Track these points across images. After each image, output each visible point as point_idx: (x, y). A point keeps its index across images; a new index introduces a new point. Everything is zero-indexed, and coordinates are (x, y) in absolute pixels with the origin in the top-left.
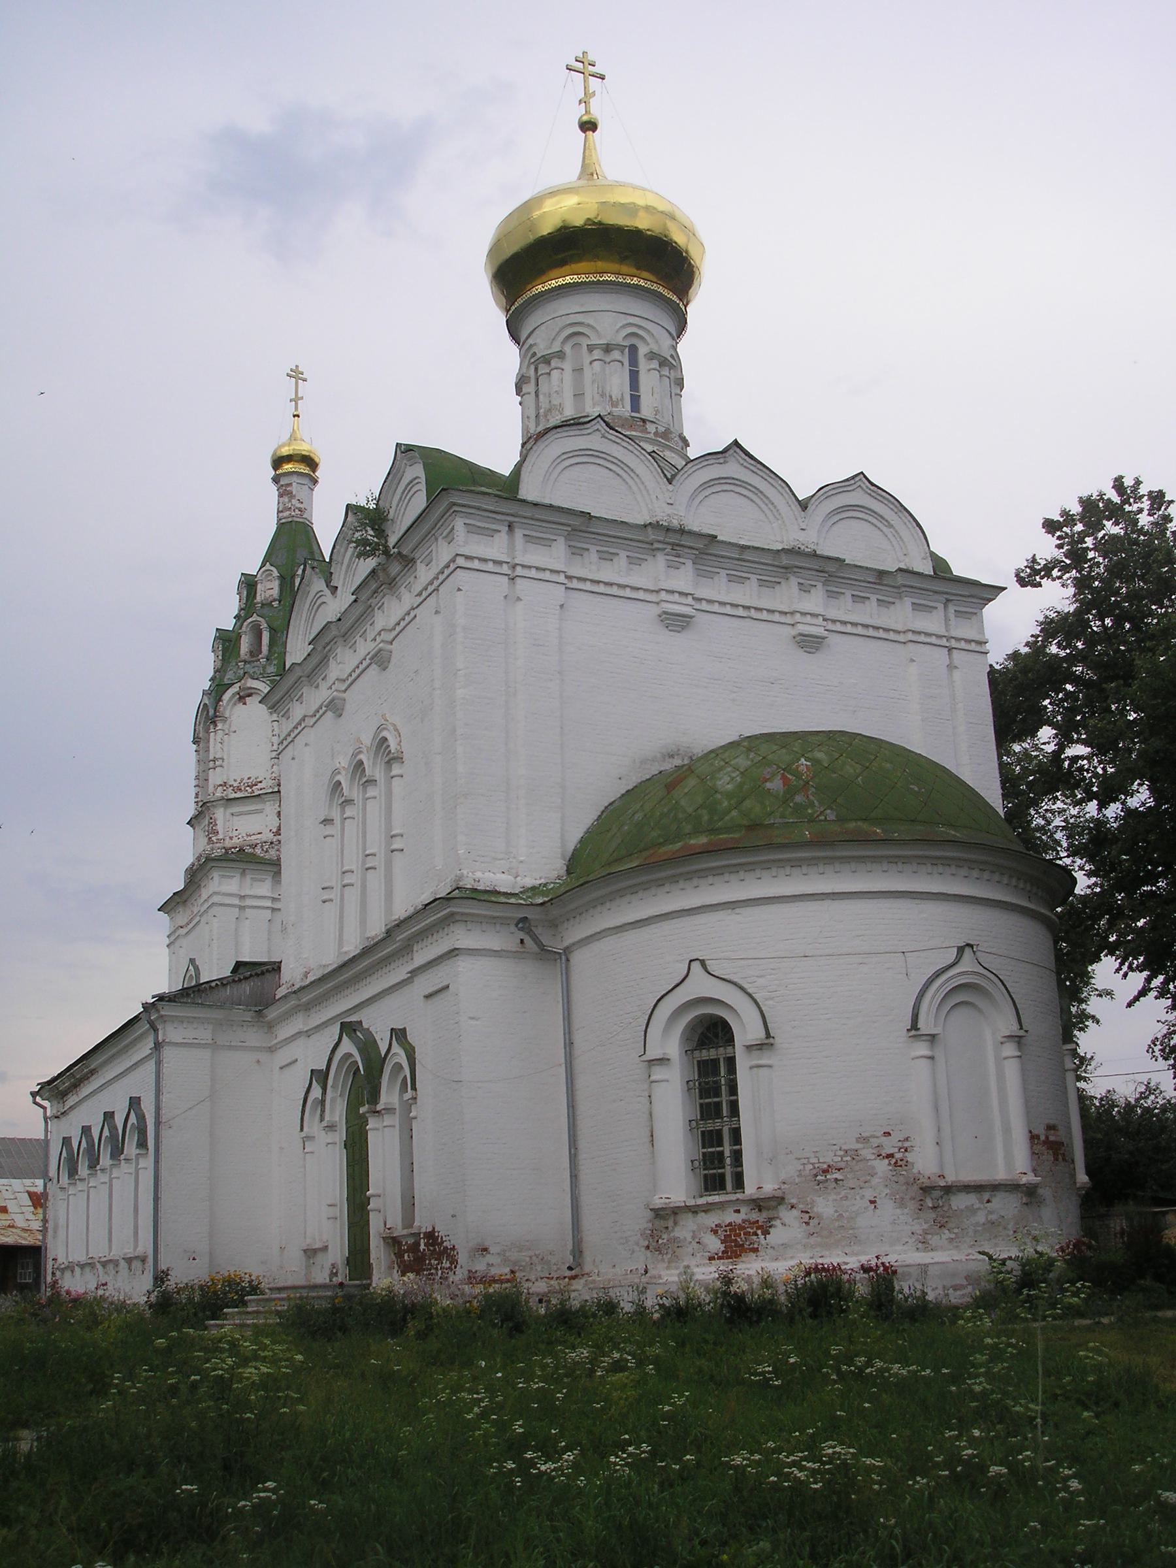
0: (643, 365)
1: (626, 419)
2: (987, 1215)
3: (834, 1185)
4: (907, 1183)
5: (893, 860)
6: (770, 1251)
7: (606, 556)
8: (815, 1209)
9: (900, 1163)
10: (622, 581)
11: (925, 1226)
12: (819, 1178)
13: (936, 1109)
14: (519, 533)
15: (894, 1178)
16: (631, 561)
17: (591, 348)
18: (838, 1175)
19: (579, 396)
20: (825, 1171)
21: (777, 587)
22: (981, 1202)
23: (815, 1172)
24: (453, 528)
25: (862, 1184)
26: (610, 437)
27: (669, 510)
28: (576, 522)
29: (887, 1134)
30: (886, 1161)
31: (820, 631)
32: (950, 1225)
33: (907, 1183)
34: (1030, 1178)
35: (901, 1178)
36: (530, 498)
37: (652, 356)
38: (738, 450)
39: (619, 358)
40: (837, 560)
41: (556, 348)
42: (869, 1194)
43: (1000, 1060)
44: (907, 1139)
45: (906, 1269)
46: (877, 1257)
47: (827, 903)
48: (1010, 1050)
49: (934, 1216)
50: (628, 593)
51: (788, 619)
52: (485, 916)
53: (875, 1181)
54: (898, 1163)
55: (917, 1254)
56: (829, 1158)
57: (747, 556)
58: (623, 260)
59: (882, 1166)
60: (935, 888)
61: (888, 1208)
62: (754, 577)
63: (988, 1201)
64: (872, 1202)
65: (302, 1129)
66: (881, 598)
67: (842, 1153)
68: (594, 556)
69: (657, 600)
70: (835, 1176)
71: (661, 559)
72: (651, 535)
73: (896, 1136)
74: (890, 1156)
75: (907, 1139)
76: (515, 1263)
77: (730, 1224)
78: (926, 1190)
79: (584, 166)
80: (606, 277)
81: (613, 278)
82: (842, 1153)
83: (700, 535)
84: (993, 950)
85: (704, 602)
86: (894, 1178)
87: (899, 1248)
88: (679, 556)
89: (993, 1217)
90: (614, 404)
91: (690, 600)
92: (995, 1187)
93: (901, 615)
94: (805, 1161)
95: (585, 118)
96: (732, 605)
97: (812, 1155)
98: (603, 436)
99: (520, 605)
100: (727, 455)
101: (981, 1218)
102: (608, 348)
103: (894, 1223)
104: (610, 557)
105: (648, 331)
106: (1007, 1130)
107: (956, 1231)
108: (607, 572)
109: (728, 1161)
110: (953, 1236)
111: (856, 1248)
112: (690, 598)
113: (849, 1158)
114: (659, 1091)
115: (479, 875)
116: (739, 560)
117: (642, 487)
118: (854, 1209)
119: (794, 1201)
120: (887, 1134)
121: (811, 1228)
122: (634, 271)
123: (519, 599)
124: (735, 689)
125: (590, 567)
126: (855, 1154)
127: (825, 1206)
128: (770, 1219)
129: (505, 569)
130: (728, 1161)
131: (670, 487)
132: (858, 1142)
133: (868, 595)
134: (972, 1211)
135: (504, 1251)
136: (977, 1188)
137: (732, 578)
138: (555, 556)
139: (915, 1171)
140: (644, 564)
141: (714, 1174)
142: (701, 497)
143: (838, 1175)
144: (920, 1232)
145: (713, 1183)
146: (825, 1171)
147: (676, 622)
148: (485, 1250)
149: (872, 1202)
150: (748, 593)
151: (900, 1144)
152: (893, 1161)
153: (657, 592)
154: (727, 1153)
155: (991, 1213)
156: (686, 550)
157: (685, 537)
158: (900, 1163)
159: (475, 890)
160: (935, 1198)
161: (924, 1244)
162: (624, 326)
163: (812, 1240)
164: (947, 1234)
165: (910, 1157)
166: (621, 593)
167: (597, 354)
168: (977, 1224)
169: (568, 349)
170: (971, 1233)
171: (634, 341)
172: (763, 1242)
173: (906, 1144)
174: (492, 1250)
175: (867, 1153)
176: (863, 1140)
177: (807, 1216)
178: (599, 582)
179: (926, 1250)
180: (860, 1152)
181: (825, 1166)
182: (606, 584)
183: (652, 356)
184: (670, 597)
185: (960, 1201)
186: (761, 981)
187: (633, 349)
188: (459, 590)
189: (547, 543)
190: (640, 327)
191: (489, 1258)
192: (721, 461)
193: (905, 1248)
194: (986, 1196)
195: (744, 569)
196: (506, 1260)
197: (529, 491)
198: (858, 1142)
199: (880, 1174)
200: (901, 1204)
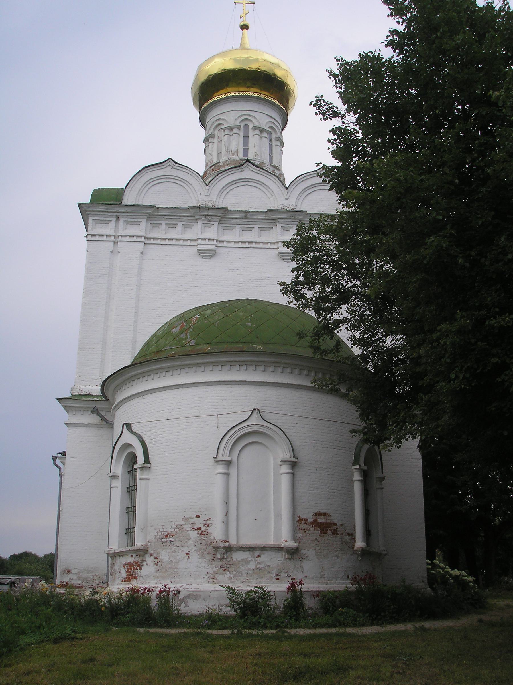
0: (251, 133)
1: (237, 160)
2: (256, 565)
3: (169, 544)
4: (207, 545)
5: (215, 364)
6: (141, 578)
7: (188, 227)
8: (160, 557)
9: (203, 533)
11: (215, 569)
12: (163, 540)
13: (227, 503)
14: (121, 220)
15: (199, 542)
17: (224, 129)
18: (172, 539)
19: (219, 154)
20: (166, 536)
21: (271, 230)
22: (253, 556)
23: (161, 537)
25: (183, 544)
26: (176, 167)
27: (207, 199)
28: (150, 211)
29: (198, 516)
30: (196, 532)
31: (214, 248)
32: (230, 569)
33: (207, 545)
34: (291, 544)
35: (204, 542)
36: (129, 203)
37: (255, 128)
38: (249, 164)
39: (266, 136)
40: (302, 212)
41: (237, 123)
42: (186, 550)
43: (277, 475)
44: (208, 520)
45: (198, 593)
46: (165, 586)
47: (181, 391)
48: (285, 469)
49: (221, 563)
50: (181, 242)
51: (275, 246)
52: (82, 407)
53: (190, 542)
54: (202, 532)
55: (207, 585)
56: (169, 529)
57: (249, 216)
58: (238, 85)
59: (194, 534)
60: (284, 381)
61: (195, 557)
62: (256, 227)
63: (258, 556)
64: (187, 554)
66: (126, 219)
67: (174, 526)
68: (163, 227)
69: (196, 244)
70: (171, 539)
71: (200, 224)
72: (197, 212)
73: (203, 518)
74: (199, 529)
75: (208, 520)
76: (85, 579)
77: (129, 563)
78: (216, 548)
79: (241, 45)
80: (230, 94)
81: (233, 94)
82: (174, 526)
83: (219, 209)
84: (281, 412)
85: (254, 244)
86: (199, 542)
87: (199, 581)
88: (210, 221)
89: (262, 566)
90: (233, 154)
91: (215, 242)
92: (264, 549)
94: (158, 530)
95: (242, 24)
96: (242, 242)
97: (161, 527)
98: (173, 168)
99: (119, 254)
100: (243, 167)
101: (252, 566)
102: (231, 128)
103: (197, 566)
105: (254, 117)
106: (278, 515)
107: (234, 573)
108: (173, 234)
110: (232, 576)
111: (177, 579)
112: (215, 241)
113: (177, 530)
115: (83, 387)
116: (246, 219)
117: (193, 190)
118: (178, 557)
119: (152, 552)
120: (198, 516)
121: (158, 567)
122: (259, 91)
123: (119, 252)
124: (240, 285)
125: (161, 232)
126: (180, 528)
127: (165, 556)
128: (143, 561)
129: (112, 238)
131: (207, 187)
132: (183, 521)
134: (246, 562)
135: (79, 572)
136: (251, 549)
137: (97, 221)
138: (141, 229)
139: (212, 538)
140: (193, 227)
142: (303, 197)
143: (172, 539)
144: (212, 572)
146: (166, 536)
147: (208, 254)
148: (69, 571)
149: (187, 554)
151: (205, 522)
152: (201, 531)
153: (197, 240)
155: (259, 563)
156: (213, 218)
157: (210, 211)
158: (203, 533)
159: (80, 395)
160: (224, 553)
161: (213, 579)
162: (240, 116)
163: (158, 574)
164: (228, 574)
165: (209, 530)
167: (227, 132)
168: (249, 569)
169: (216, 133)
170: (244, 575)
171: (246, 122)
172: (139, 573)
173: (208, 522)
174: (73, 572)
175: (187, 527)
176: (186, 519)
177: (157, 560)
179: (213, 583)
180: (183, 526)
181: (166, 534)
183: (255, 128)
184: (203, 242)
185: (238, 556)
186: (149, 433)
187: (246, 126)
189: (137, 223)
190: (249, 115)
191: (70, 576)
192: (239, 170)
193: (202, 581)
194: (257, 553)
196: (79, 577)
197: (128, 199)
198: (183, 521)
199: (192, 539)
200: (202, 556)
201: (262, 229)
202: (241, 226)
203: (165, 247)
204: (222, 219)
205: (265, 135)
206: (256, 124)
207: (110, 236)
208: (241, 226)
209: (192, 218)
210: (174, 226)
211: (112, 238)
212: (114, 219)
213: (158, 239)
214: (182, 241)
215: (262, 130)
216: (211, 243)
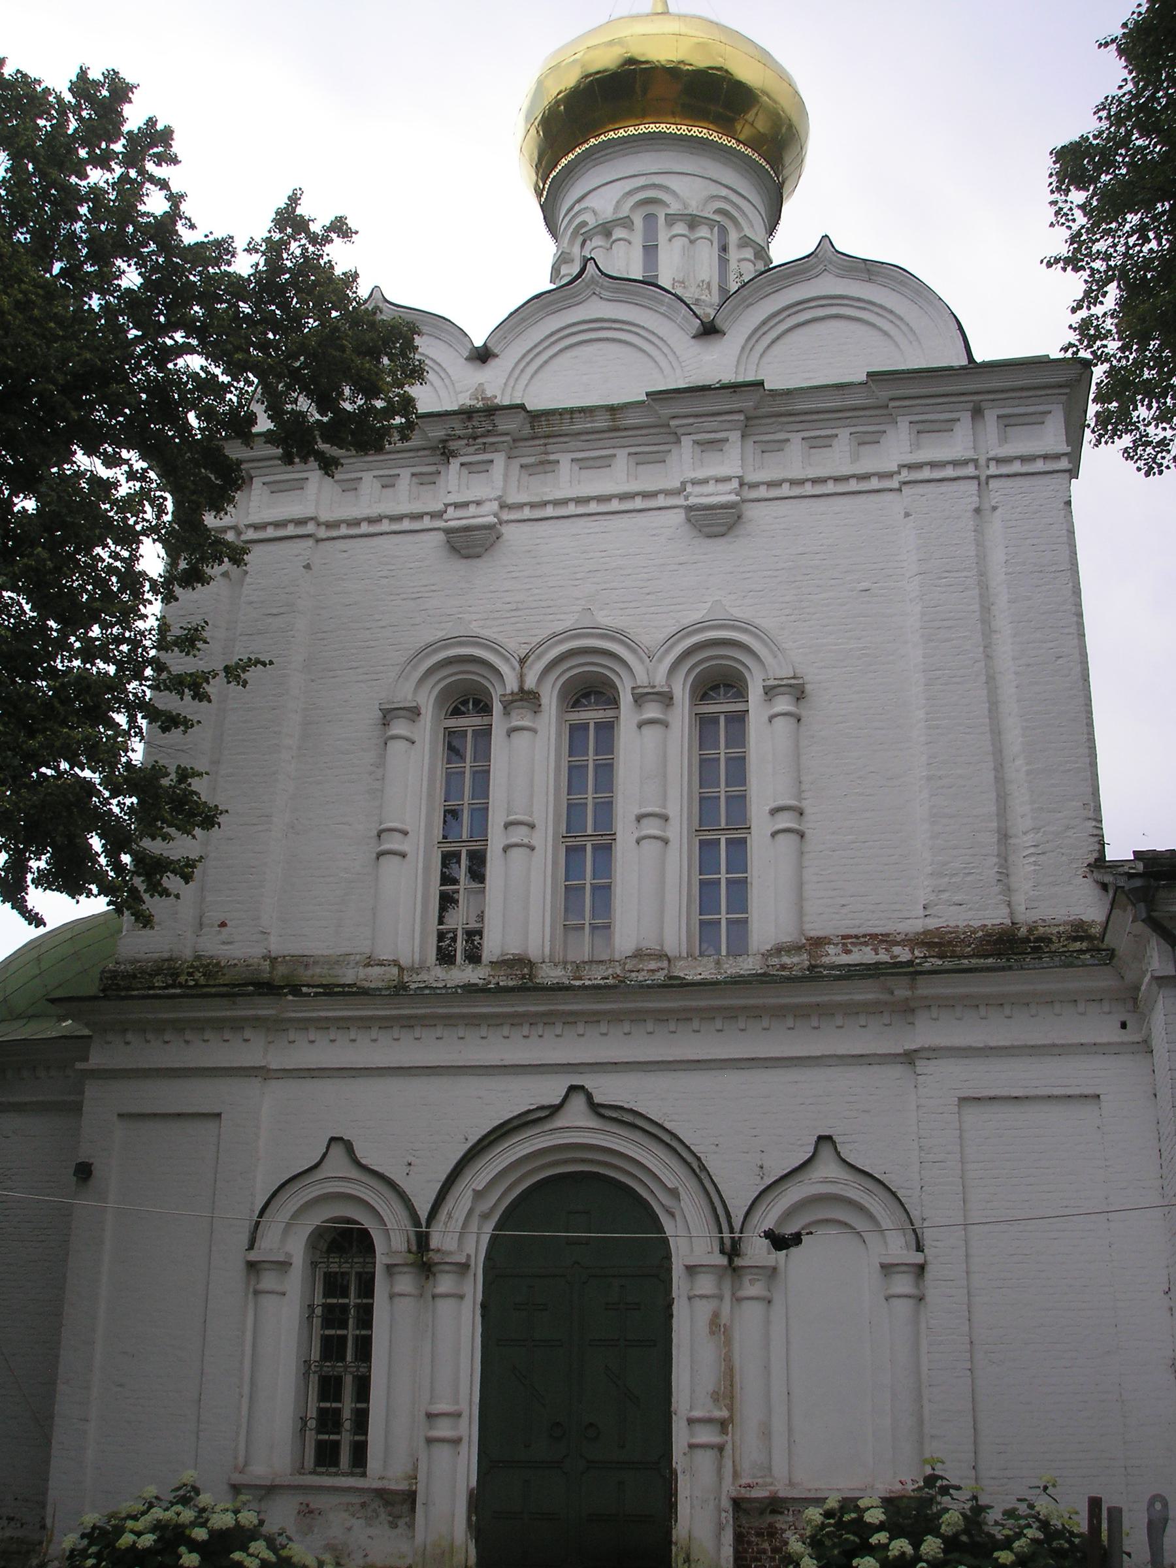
7: (868, 438)
10: (812, 473)
14: (991, 416)
16: (1007, 422)
24: (788, 440)
39: (600, 243)
41: (625, 211)
65: (251, 1247)
72: (883, 393)
85: (386, 522)
93: (897, 447)
104: (431, 478)
109: (347, 1425)
114: (708, 1379)
130: (347, 1425)
133: (834, 432)
137: (640, 458)
141: (326, 1441)
145: (326, 1456)
150: (618, 477)
154: (347, 1414)
162: (630, 193)
166: (281, 533)
178: (545, 504)
182: (837, 479)
183: (671, 220)
187: (650, 218)
188: (907, 515)
195: (918, 409)
201: (920, 427)
202: (633, 450)
203: (945, 488)
204: (517, 444)
205: (703, 231)
206: (675, 207)
207: (966, 463)
208: (633, 450)
209: (662, 430)
210: (825, 442)
211: (970, 470)
212: (966, 417)
213: (545, 504)
214: (831, 484)
215: (693, 222)
216: (723, 487)
